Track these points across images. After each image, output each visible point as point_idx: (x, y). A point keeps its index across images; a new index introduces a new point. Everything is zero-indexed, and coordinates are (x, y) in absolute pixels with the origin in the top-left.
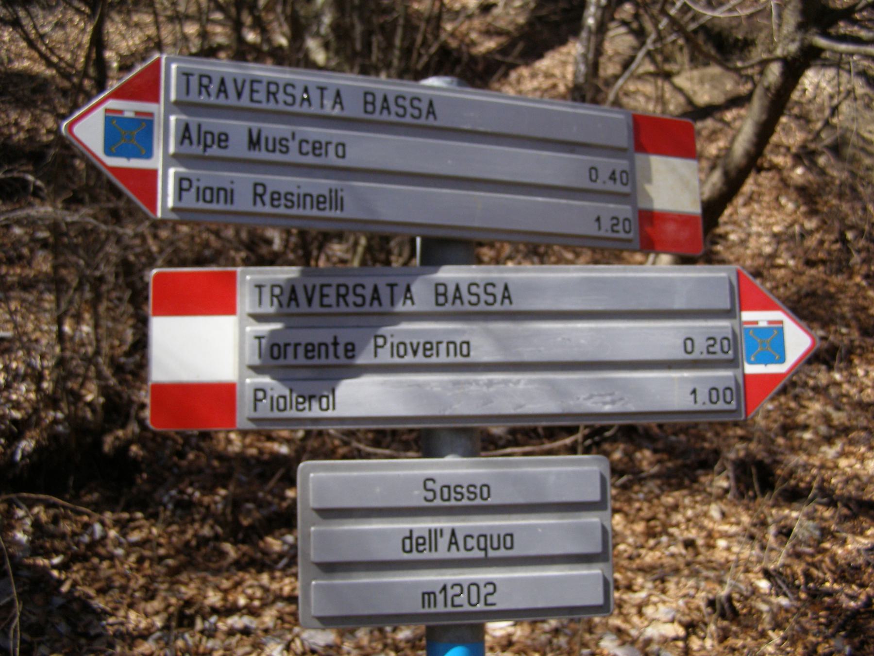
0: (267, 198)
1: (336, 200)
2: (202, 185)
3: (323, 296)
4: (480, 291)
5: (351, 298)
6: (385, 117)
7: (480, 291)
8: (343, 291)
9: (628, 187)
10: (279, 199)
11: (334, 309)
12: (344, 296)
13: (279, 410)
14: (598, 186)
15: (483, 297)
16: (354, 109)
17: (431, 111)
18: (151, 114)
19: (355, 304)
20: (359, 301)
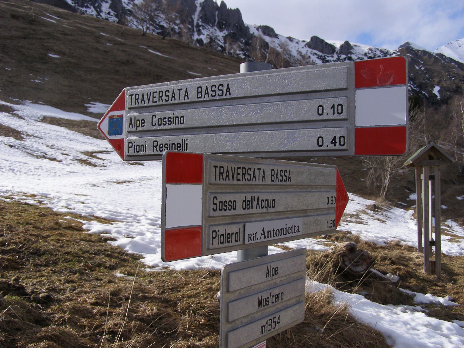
0: (158, 147)
1: (184, 144)
2: (136, 144)
3: (154, 97)
4: (216, 89)
5: (164, 97)
6: (207, 98)
7: (216, 89)
8: (161, 95)
9: (344, 113)
10: (162, 147)
11: (158, 103)
12: (161, 97)
13: (137, 152)
14: (324, 117)
15: (218, 92)
16: (193, 96)
17: (228, 91)
18: (122, 115)
19: (166, 101)
20: (167, 98)
